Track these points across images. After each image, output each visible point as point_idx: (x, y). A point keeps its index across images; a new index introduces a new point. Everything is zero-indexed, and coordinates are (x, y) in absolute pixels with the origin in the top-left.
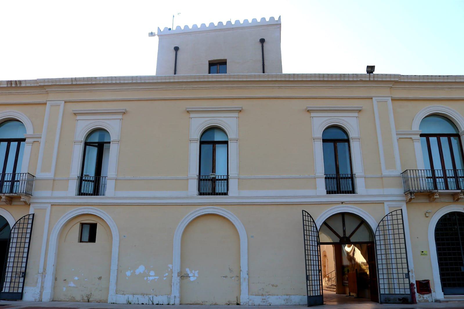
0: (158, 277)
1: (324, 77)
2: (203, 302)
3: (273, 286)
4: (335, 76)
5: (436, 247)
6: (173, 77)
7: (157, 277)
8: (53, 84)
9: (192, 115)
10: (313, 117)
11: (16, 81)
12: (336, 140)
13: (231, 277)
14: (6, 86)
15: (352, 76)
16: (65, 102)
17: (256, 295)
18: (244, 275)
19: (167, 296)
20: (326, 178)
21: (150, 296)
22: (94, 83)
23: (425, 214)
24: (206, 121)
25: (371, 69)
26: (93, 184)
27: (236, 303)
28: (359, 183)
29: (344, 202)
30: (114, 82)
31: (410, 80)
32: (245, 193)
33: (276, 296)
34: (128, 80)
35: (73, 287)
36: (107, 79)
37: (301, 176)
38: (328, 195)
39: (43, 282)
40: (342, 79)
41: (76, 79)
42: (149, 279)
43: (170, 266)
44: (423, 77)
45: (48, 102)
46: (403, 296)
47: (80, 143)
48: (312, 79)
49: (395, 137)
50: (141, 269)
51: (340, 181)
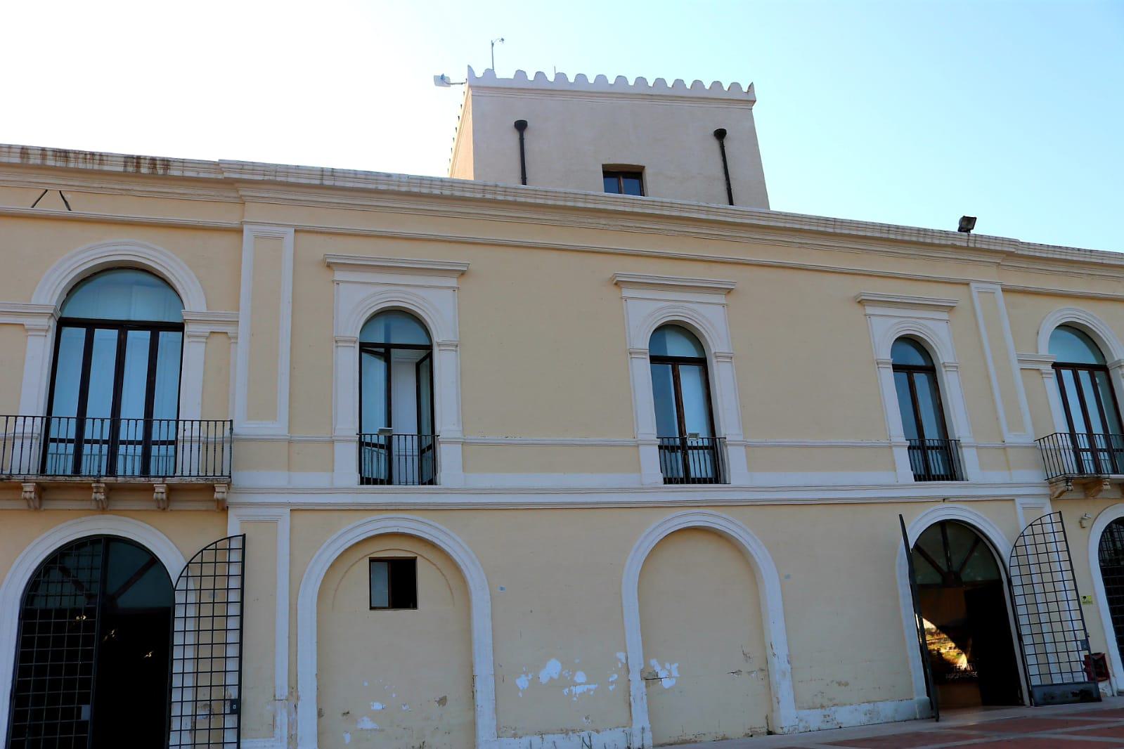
0: (596, 685)
1: (889, 230)
2: (696, 737)
3: (840, 684)
4: (909, 231)
5: (1106, 588)
6: (563, 195)
7: (593, 687)
8: (266, 178)
9: (339, 275)
10: (870, 315)
11: (153, 160)
12: (916, 365)
13: (750, 673)
14: (121, 169)
15: (939, 235)
16: (295, 231)
17: (809, 709)
18: (779, 664)
19: (622, 729)
20: (909, 448)
21: (582, 734)
22: (382, 187)
23: (1080, 522)
24: (662, 308)
25: (967, 223)
26: (399, 455)
27: (765, 730)
28: (969, 459)
29: (948, 498)
30: (437, 192)
31: (1032, 254)
32: (762, 479)
33: (848, 707)
34: (545, 198)
35: (371, 730)
36: (419, 181)
37: (864, 441)
38: (919, 482)
39: (292, 725)
40: (921, 240)
41: (333, 172)
42: (574, 693)
43: (621, 655)
44: (1053, 249)
45: (246, 228)
46: (1081, 687)
47: (44, 334)
48: (869, 234)
49: (1016, 366)
50: (553, 669)
51: (936, 457)
